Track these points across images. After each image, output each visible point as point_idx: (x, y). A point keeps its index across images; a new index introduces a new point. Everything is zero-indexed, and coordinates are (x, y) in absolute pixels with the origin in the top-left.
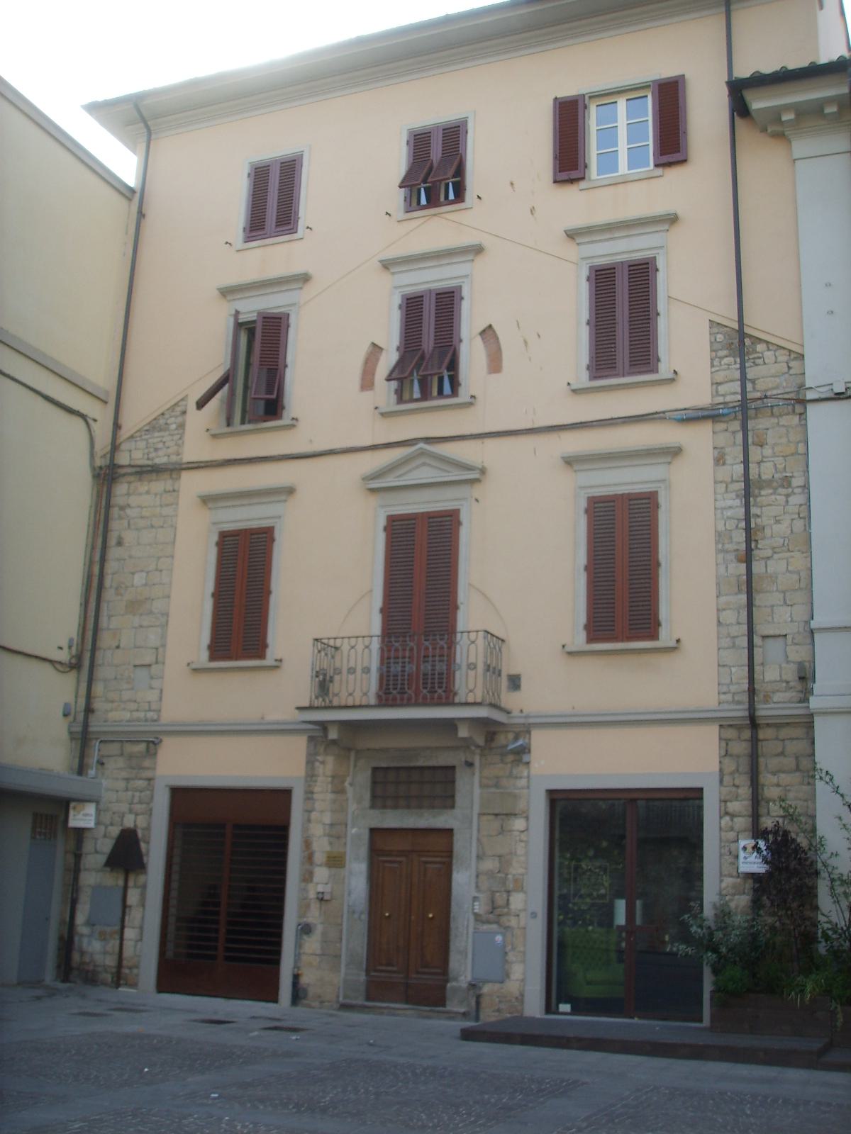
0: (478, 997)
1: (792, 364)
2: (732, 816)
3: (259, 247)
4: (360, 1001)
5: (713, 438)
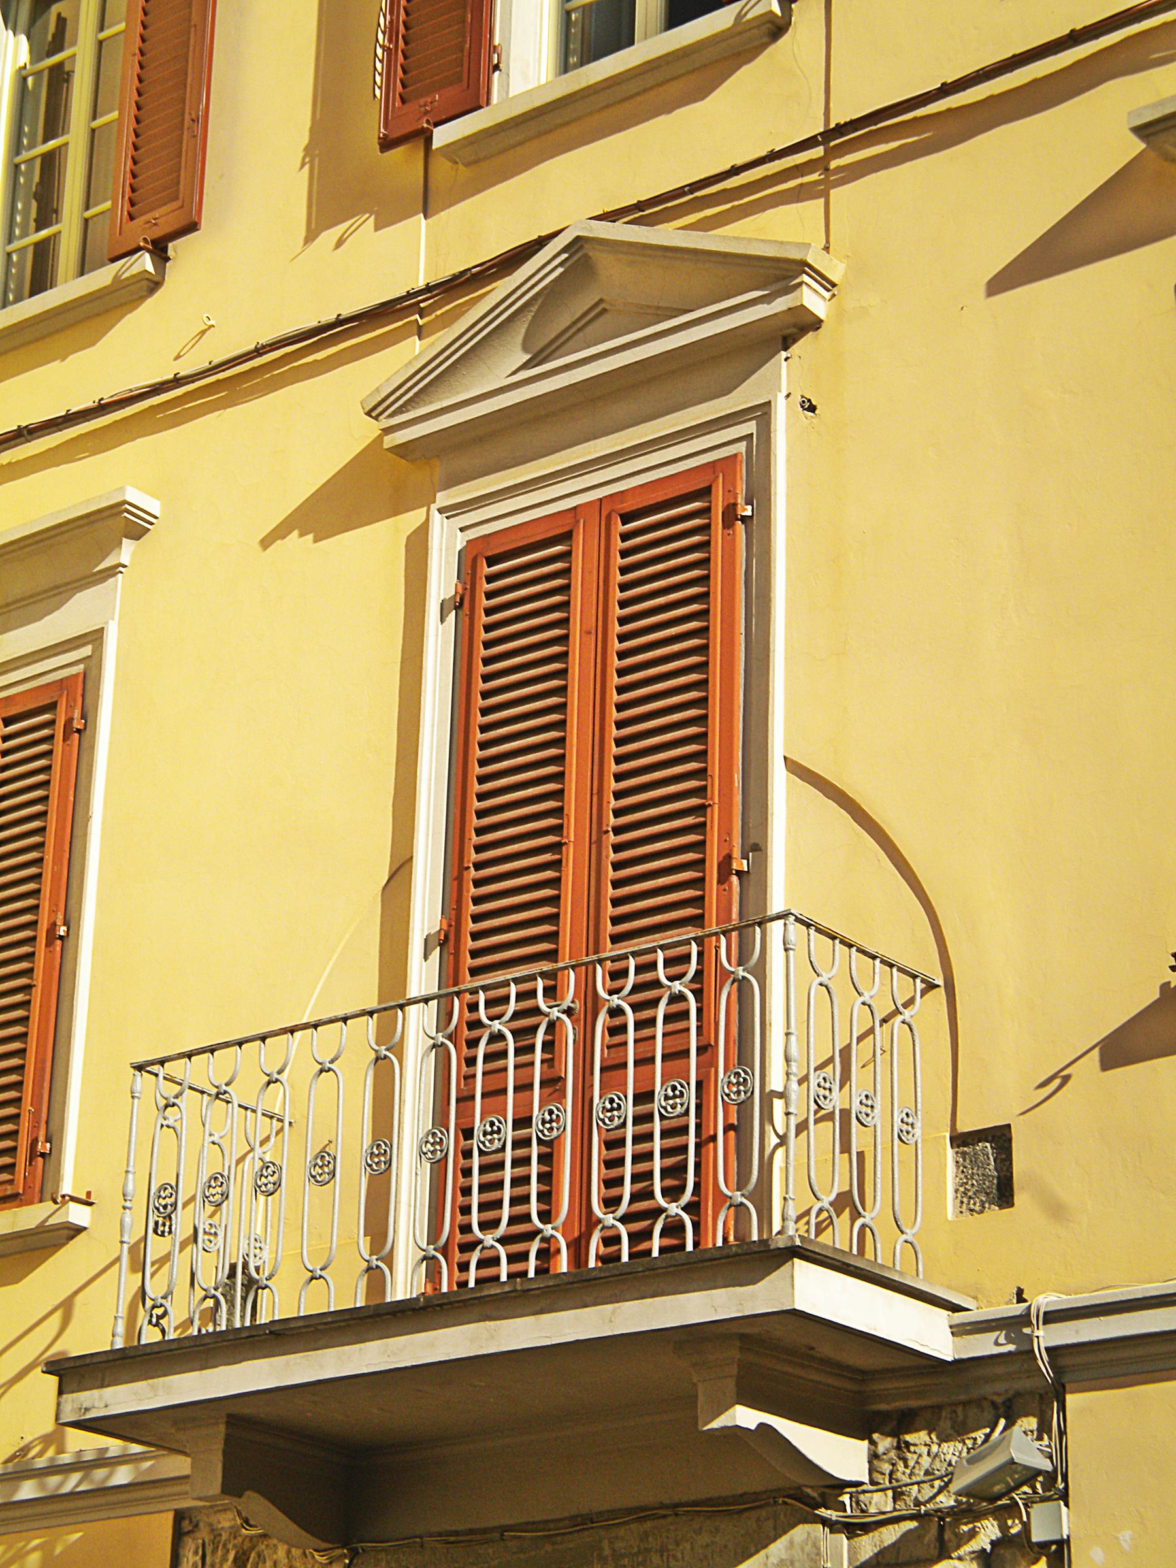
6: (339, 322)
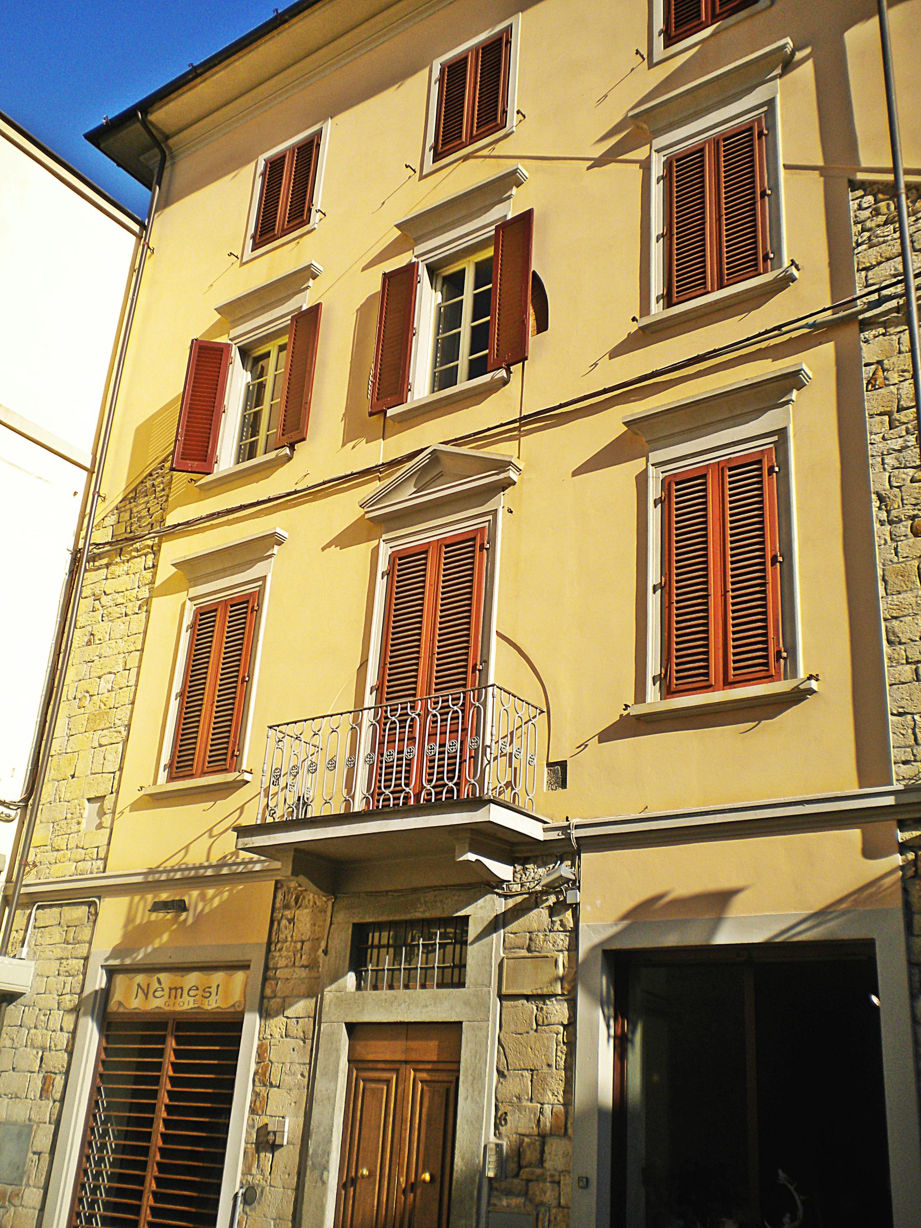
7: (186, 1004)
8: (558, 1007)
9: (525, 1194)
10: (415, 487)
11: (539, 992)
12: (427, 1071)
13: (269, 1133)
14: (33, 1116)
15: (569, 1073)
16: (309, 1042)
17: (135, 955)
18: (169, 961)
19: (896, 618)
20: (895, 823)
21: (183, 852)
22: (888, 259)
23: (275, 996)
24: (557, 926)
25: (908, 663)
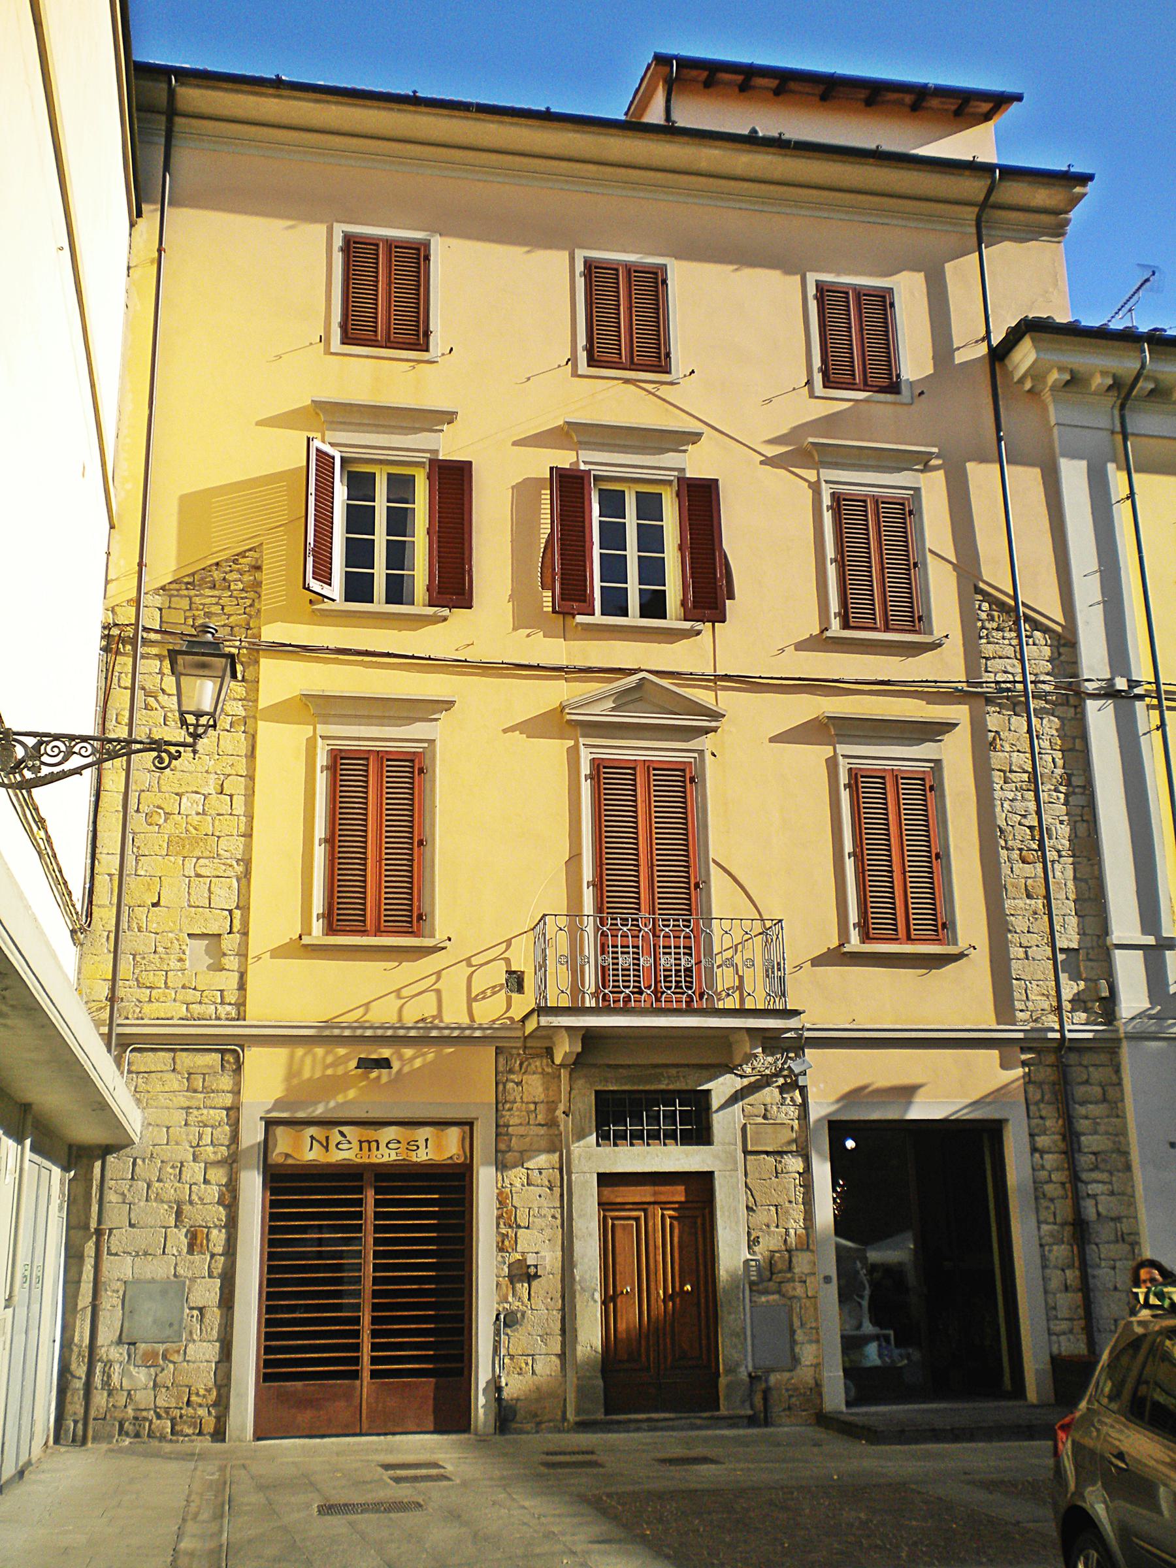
0: (766, 1393)
1: (1062, 650)
2: (1042, 1153)
3: (367, 357)
4: (600, 1416)
5: (406, 604)
6: (538, 666)
7: (386, 1156)
8: (793, 1160)
9: (779, 1292)
10: (614, 702)
11: (780, 1149)
12: (673, 1209)
13: (529, 1266)
14: (180, 1271)
15: (807, 1207)
16: (557, 1190)
17: (311, 1110)
18: (364, 1115)
19: (1012, 915)
20: (1018, 1049)
21: (361, 1010)
22: (1000, 658)
23: (510, 1151)
24: (788, 1101)
25: (1021, 946)
